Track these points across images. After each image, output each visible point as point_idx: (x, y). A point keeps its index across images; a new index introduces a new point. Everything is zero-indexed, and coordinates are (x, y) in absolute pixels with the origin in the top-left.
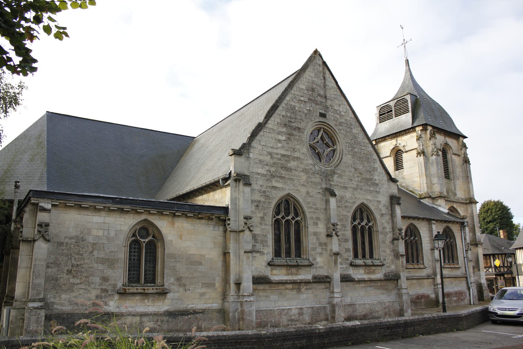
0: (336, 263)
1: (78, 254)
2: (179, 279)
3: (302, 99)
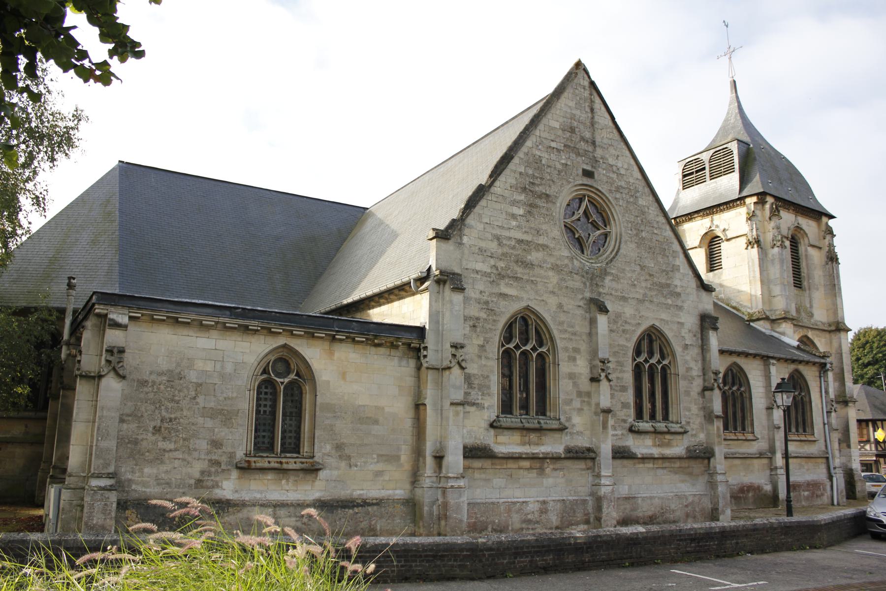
0: (605, 426)
1: (172, 400)
2: (339, 447)
3: (553, 145)
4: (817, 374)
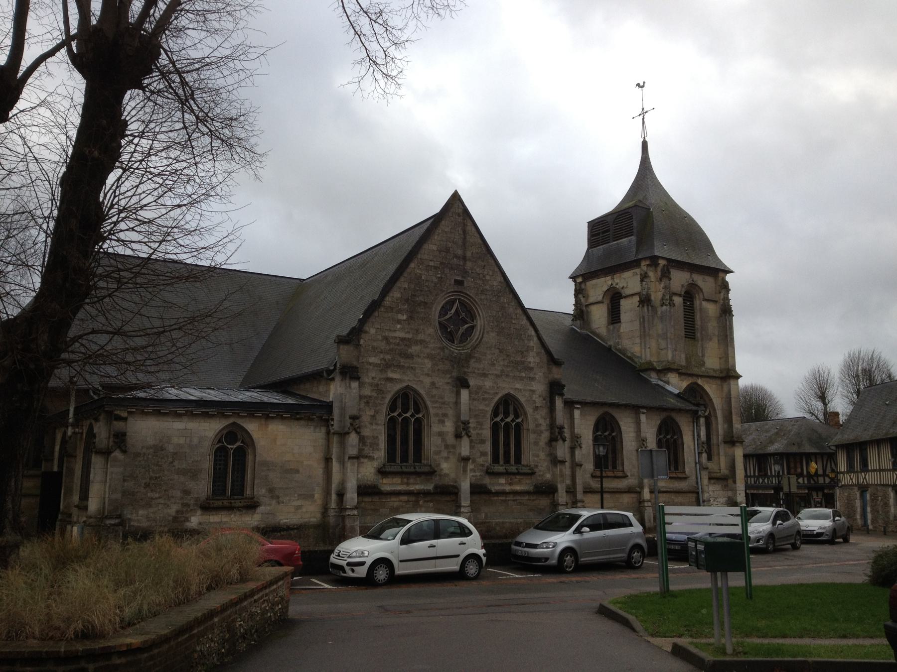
0: (465, 471)
1: (157, 465)
2: (271, 490)
3: (432, 264)
4: (690, 419)
